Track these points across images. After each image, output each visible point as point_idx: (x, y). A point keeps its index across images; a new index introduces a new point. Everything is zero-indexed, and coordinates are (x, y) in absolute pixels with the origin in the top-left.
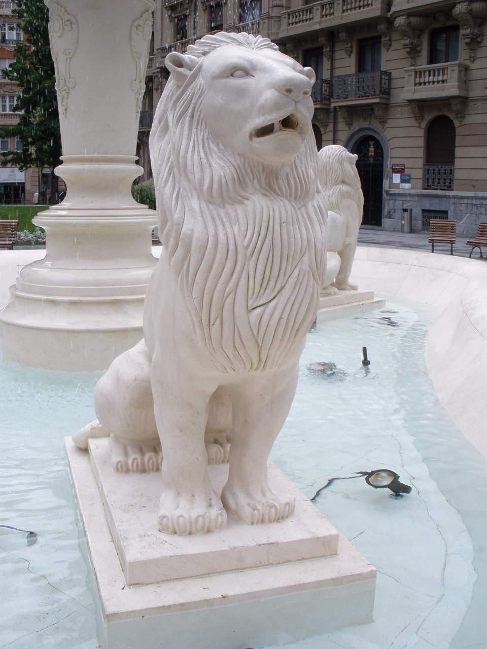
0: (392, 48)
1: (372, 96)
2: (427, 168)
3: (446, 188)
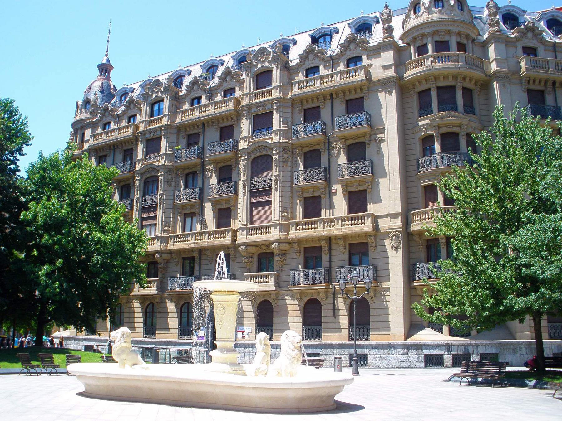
0: (236, 261)
1: (319, 284)
2: (307, 328)
3: (364, 340)
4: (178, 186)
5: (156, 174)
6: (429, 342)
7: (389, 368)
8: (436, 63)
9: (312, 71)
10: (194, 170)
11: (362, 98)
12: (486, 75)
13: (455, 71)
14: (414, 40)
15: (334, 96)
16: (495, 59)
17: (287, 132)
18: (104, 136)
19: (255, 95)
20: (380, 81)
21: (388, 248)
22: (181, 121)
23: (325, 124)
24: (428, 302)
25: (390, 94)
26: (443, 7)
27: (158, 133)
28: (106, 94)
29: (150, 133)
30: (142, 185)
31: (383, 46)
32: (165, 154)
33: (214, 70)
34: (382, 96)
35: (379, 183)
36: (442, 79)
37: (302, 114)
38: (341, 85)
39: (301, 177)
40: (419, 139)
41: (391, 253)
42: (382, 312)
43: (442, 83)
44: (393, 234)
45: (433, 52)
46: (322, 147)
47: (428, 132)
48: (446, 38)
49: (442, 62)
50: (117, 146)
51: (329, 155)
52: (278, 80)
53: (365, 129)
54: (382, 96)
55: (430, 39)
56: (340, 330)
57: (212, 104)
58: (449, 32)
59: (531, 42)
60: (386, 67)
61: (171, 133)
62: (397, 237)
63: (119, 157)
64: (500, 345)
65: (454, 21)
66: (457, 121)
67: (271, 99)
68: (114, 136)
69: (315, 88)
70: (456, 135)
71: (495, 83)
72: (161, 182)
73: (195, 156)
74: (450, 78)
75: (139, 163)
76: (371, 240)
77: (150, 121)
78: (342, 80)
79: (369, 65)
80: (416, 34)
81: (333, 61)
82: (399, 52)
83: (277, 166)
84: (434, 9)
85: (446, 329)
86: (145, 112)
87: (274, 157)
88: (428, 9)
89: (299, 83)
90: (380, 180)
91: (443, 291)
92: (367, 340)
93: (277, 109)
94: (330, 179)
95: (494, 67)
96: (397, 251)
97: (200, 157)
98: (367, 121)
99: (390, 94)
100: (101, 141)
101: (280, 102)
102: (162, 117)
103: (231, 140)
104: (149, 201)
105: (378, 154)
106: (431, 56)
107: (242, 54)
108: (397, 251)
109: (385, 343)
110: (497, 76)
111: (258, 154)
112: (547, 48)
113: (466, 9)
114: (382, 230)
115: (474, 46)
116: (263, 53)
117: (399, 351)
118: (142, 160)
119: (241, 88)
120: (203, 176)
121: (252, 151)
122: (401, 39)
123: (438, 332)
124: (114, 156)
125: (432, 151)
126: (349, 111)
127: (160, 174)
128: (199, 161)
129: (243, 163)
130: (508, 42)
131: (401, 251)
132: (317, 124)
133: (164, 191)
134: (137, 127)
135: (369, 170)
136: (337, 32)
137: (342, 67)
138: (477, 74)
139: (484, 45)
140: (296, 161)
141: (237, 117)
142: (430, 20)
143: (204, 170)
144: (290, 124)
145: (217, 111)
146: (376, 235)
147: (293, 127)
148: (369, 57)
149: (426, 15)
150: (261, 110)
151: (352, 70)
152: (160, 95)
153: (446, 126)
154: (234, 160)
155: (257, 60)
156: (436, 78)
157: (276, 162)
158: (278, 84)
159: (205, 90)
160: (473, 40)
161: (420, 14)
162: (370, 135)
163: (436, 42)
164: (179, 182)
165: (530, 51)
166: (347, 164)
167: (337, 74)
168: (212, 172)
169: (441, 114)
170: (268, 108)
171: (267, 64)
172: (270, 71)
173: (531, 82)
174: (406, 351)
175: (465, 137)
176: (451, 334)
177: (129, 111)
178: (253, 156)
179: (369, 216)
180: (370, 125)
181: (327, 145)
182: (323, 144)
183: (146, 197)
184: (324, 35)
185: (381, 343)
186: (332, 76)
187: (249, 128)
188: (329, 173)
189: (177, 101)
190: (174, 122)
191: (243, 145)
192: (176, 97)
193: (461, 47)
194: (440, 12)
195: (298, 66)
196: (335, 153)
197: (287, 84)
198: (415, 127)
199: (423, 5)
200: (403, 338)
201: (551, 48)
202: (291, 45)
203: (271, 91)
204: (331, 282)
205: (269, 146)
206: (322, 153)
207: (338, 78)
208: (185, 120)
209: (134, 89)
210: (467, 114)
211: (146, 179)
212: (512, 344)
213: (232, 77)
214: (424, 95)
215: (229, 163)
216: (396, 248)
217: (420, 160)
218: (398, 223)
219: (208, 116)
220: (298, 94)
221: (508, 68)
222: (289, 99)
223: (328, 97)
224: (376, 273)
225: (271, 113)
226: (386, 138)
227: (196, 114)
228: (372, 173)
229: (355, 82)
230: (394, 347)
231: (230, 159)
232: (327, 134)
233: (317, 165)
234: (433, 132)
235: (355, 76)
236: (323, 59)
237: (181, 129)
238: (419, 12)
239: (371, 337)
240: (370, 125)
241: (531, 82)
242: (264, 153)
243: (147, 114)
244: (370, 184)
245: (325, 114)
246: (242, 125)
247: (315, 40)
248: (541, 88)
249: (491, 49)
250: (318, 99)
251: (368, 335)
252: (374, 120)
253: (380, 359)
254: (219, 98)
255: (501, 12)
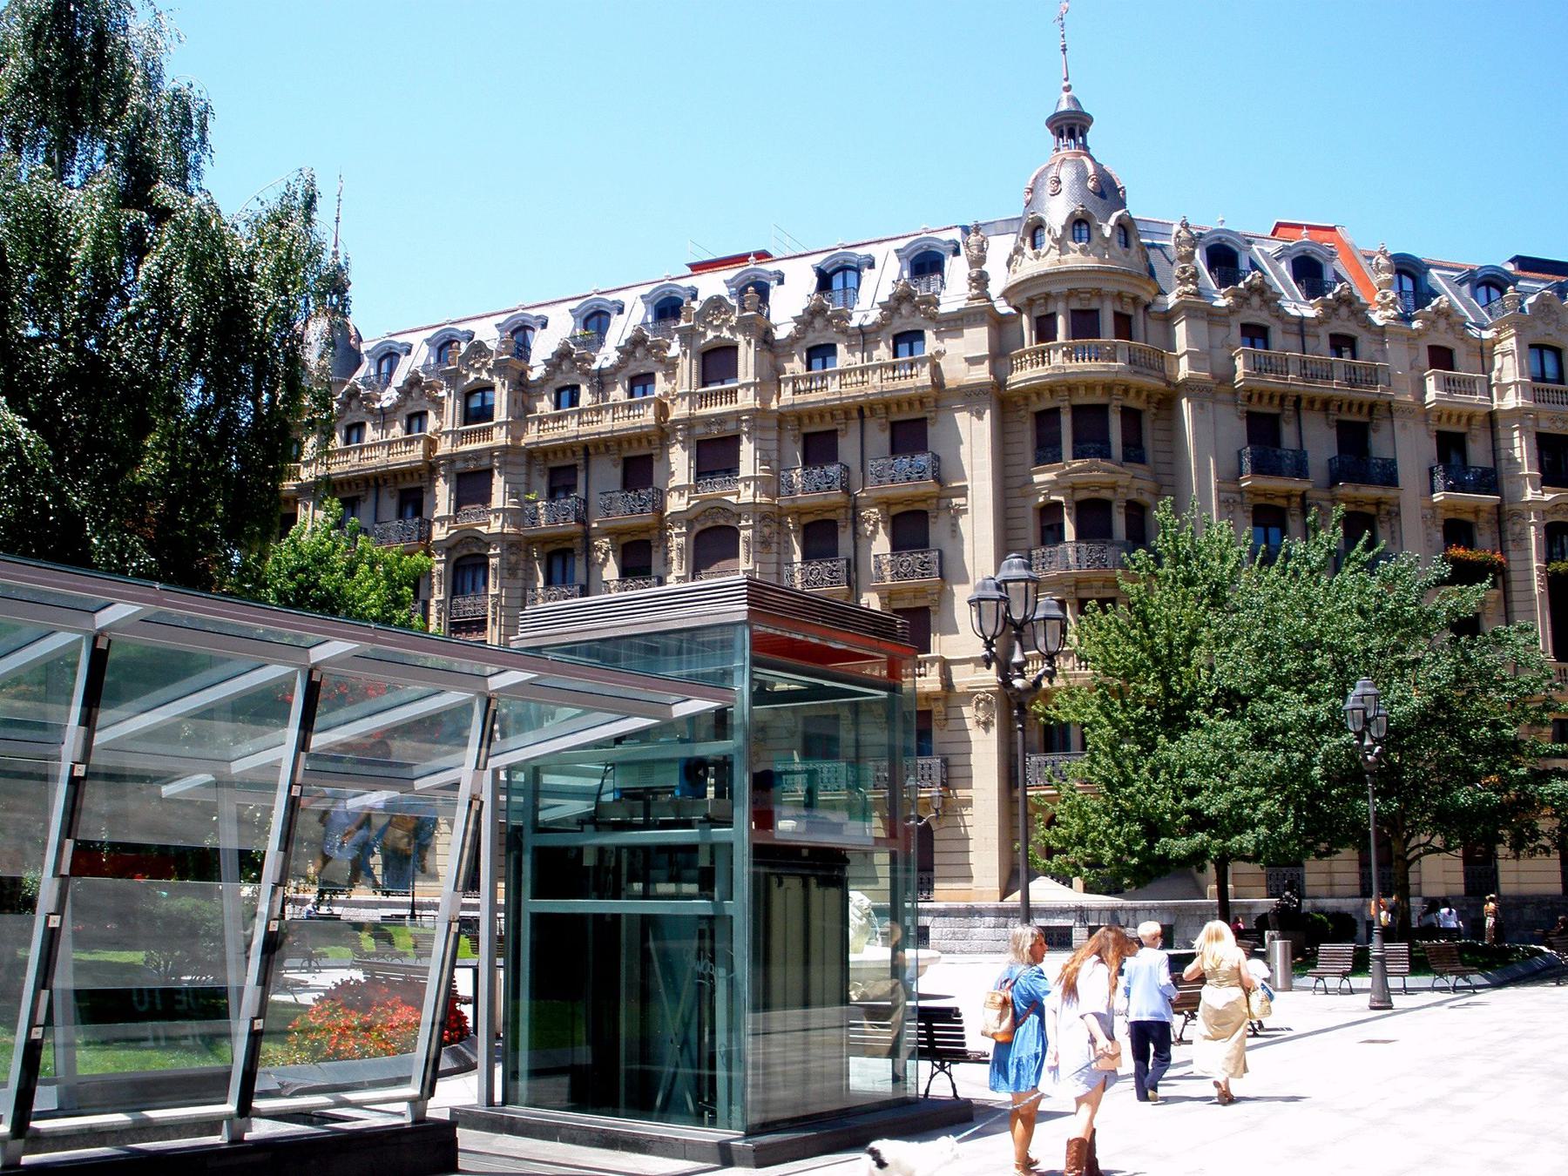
4: (531, 577)
5: (483, 552)
6: (1047, 905)
7: (970, 952)
8: (1071, 360)
9: (821, 353)
10: (568, 545)
11: (924, 419)
12: (1169, 383)
13: (1109, 378)
14: (1031, 302)
15: (867, 412)
16: (1187, 352)
17: (773, 482)
18: (354, 458)
19: (701, 397)
20: (959, 389)
21: (970, 723)
22: (536, 440)
23: (847, 469)
24: (1044, 837)
25: (980, 417)
26: (1089, 238)
27: (485, 462)
28: (339, 350)
29: (466, 460)
30: (450, 573)
31: (968, 315)
32: (503, 510)
33: (599, 322)
34: (963, 419)
35: (953, 595)
36: (1082, 391)
37: (800, 444)
38: (882, 392)
39: (798, 576)
40: (1035, 509)
41: (975, 734)
42: (956, 846)
43: (1082, 399)
44: (981, 696)
45: (1067, 338)
46: (839, 515)
47: (1052, 498)
48: (1094, 305)
49: (1083, 360)
50: (385, 481)
51: (855, 533)
52: (751, 370)
53: (929, 486)
54: (963, 419)
55: (1061, 306)
56: (875, 880)
57: (607, 408)
58: (1098, 293)
59: (1259, 317)
60: (973, 361)
61: (512, 463)
62: (989, 703)
63: (389, 505)
64: (1176, 907)
65: (1110, 271)
66: (1109, 479)
67: (737, 412)
68: (378, 459)
69: (828, 394)
70: (1104, 506)
71: (1184, 401)
72: (495, 569)
73: (571, 518)
74: (1099, 391)
75: (442, 525)
76: (937, 708)
77: (462, 433)
78: (885, 382)
79: (938, 352)
80: (1035, 292)
81: (864, 338)
82: (1000, 326)
83: (749, 552)
84: (1070, 244)
85: (1077, 882)
86: (451, 411)
87: (743, 533)
88: (1060, 242)
89: (795, 380)
90: (956, 588)
91: (1067, 823)
92: (928, 900)
93: (748, 433)
94: (857, 582)
95: (1184, 370)
96: (987, 730)
97: (583, 520)
98: (934, 472)
99: (980, 417)
100: (346, 467)
101: (754, 419)
102: (492, 427)
103: (650, 490)
104: (467, 606)
105: (954, 537)
106: (1063, 345)
107: (664, 293)
108: (987, 730)
109: (962, 905)
110: (1189, 387)
111: (709, 524)
112: (1288, 327)
113: (1133, 243)
114: (958, 689)
115: (1149, 321)
116: (718, 308)
117: (990, 920)
118: (448, 518)
119: (669, 376)
120: (587, 561)
121: (696, 518)
122: (1006, 295)
123: (1064, 884)
124: (377, 498)
125: (1060, 538)
126: (895, 450)
127: (492, 551)
128: (579, 528)
129: (677, 540)
130: (1213, 316)
131: (994, 731)
132: (833, 470)
133: (501, 588)
134: (431, 444)
135: (936, 569)
136: (872, 266)
137: (883, 353)
138: (1153, 383)
139: (1168, 318)
140: (787, 542)
141: (661, 439)
142: (1063, 267)
143: (588, 549)
144: (774, 464)
145: (619, 425)
146: (946, 698)
147: (782, 473)
148: (939, 335)
149: (1055, 253)
150: (715, 432)
151: (904, 362)
152: (485, 376)
153: (1086, 487)
154: (656, 532)
155: (704, 322)
156: (1071, 389)
157: (747, 543)
158: (751, 379)
159: (587, 373)
160: (1147, 307)
161: (1043, 251)
162: (939, 498)
163: (1073, 311)
164: (534, 568)
165: (1255, 334)
166: (892, 555)
167: (874, 368)
168: (606, 554)
169: (1078, 464)
170: (730, 428)
171: (726, 334)
172: (734, 348)
173: (1255, 398)
174: (1002, 920)
175: (1123, 510)
176: (1088, 889)
177: (410, 404)
178: (698, 527)
179: (933, 660)
180: (938, 479)
181: (851, 512)
182: (843, 511)
183: (459, 600)
184: (844, 269)
185: (954, 905)
186: (863, 371)
187: (690, 468)
188: (856, 570)
189: (524, 390)
190: (520, 439)
191: (676, 504)
192: (521, 384)
193: (1124, 326)
194: (1083, 250)
195: (792, 340)
196: (866, 530)
197: (771, 379)
198: (1025, 484)
199: (1049, 232)
200: (998, 896)
201: (1295, 328)
202: (773, 283)
203: (734, 391)
204: (858, 785)
205: (733, 508)
206: (840, 530)
207: (877, 377)
208: (546, 438)
209: (411, 346)
210: (1128, 464)
211: (459, 560)
212: (1199, 906)
213: (649, 350)
214: (1046, 421)
215: (644, 536)
216: (986, 725)
217: (1034, 553)
218: (991, 676)
219: (599, 433)
220: (793, 405)
221: (1211, 373)
222: (774, 411)
223: (855, 414)
224: (947, 771)
225: (735, 440)
226: (969, 507)
227: (571, 428)
228: (941, 576)
229: (910, 389)
230: (980, 913)
231: (647, 529)
232: (851, 488)
233: (831, 553)
234: (1061, 499)
235: (912, 376)
236: (844, 332)
237: (534, 455)
238: (1041, 244)
239: (936, 895)
240: (938, 479)
241: (1255, 398)
242: (722, 522)
243: (457, 418)
244: (936, 597)
245: (848, 448)
246: (672, 458)
247: (825, 281)
248: (1274, 410)
249: (1181, 330)
250: (833, 416)
251: (931, 889)
252: (946, 468)
253: (954, 935)
254: (619, 394)
255: (1204, 244)
